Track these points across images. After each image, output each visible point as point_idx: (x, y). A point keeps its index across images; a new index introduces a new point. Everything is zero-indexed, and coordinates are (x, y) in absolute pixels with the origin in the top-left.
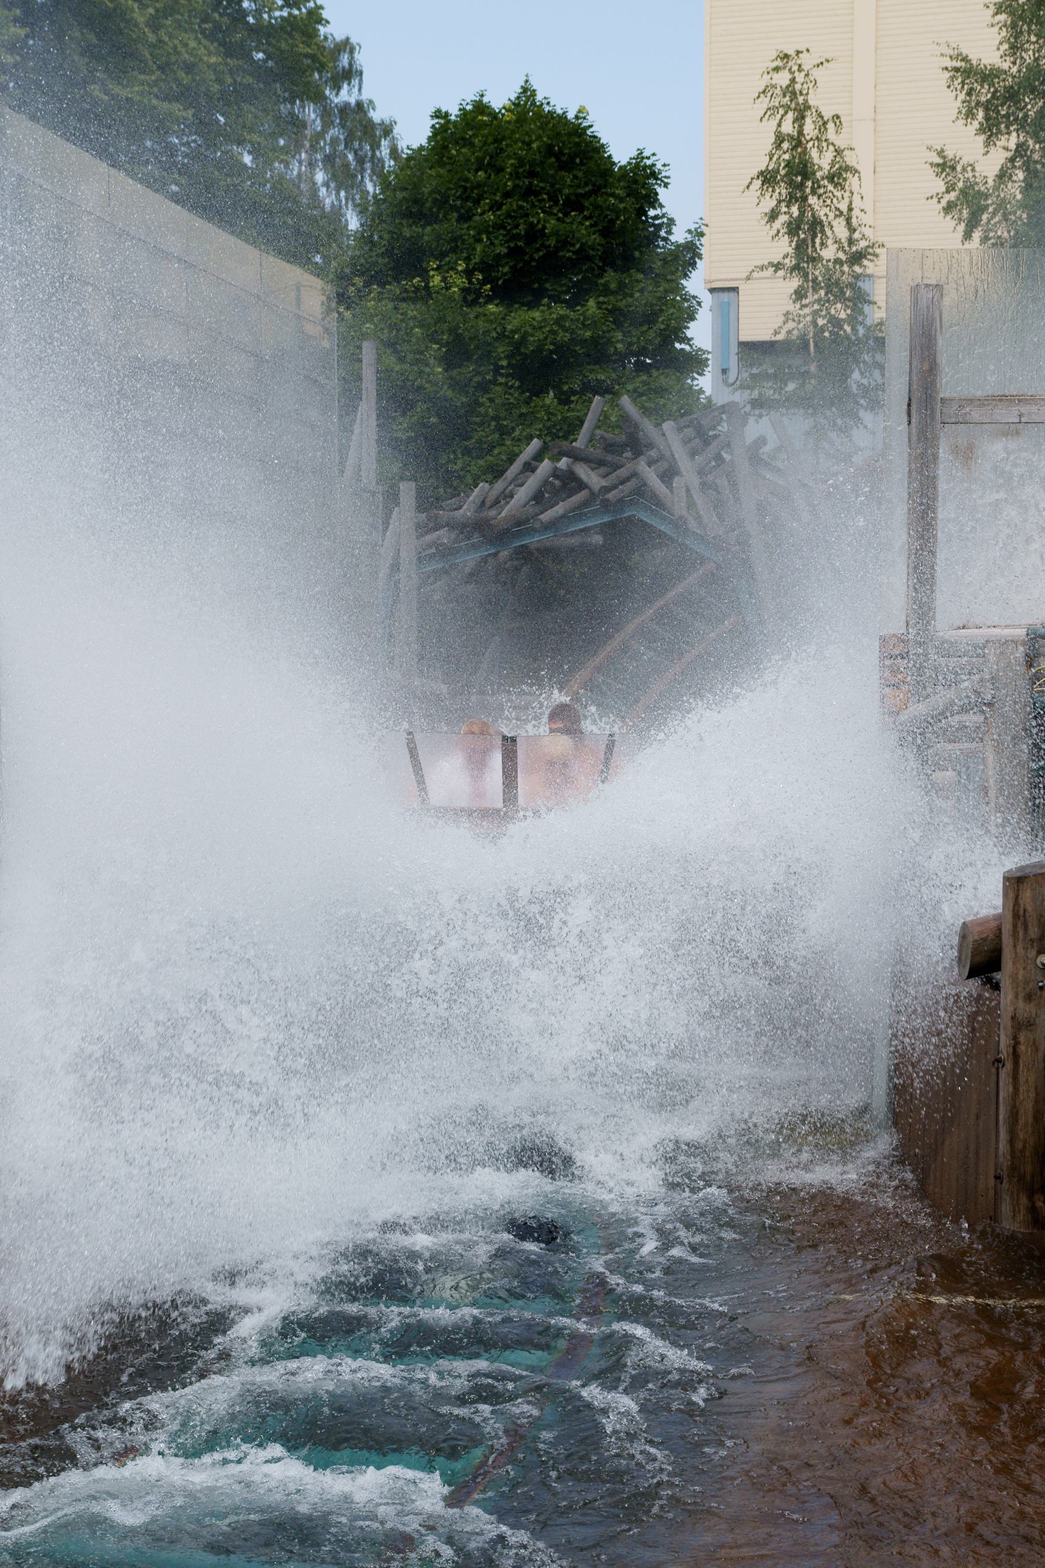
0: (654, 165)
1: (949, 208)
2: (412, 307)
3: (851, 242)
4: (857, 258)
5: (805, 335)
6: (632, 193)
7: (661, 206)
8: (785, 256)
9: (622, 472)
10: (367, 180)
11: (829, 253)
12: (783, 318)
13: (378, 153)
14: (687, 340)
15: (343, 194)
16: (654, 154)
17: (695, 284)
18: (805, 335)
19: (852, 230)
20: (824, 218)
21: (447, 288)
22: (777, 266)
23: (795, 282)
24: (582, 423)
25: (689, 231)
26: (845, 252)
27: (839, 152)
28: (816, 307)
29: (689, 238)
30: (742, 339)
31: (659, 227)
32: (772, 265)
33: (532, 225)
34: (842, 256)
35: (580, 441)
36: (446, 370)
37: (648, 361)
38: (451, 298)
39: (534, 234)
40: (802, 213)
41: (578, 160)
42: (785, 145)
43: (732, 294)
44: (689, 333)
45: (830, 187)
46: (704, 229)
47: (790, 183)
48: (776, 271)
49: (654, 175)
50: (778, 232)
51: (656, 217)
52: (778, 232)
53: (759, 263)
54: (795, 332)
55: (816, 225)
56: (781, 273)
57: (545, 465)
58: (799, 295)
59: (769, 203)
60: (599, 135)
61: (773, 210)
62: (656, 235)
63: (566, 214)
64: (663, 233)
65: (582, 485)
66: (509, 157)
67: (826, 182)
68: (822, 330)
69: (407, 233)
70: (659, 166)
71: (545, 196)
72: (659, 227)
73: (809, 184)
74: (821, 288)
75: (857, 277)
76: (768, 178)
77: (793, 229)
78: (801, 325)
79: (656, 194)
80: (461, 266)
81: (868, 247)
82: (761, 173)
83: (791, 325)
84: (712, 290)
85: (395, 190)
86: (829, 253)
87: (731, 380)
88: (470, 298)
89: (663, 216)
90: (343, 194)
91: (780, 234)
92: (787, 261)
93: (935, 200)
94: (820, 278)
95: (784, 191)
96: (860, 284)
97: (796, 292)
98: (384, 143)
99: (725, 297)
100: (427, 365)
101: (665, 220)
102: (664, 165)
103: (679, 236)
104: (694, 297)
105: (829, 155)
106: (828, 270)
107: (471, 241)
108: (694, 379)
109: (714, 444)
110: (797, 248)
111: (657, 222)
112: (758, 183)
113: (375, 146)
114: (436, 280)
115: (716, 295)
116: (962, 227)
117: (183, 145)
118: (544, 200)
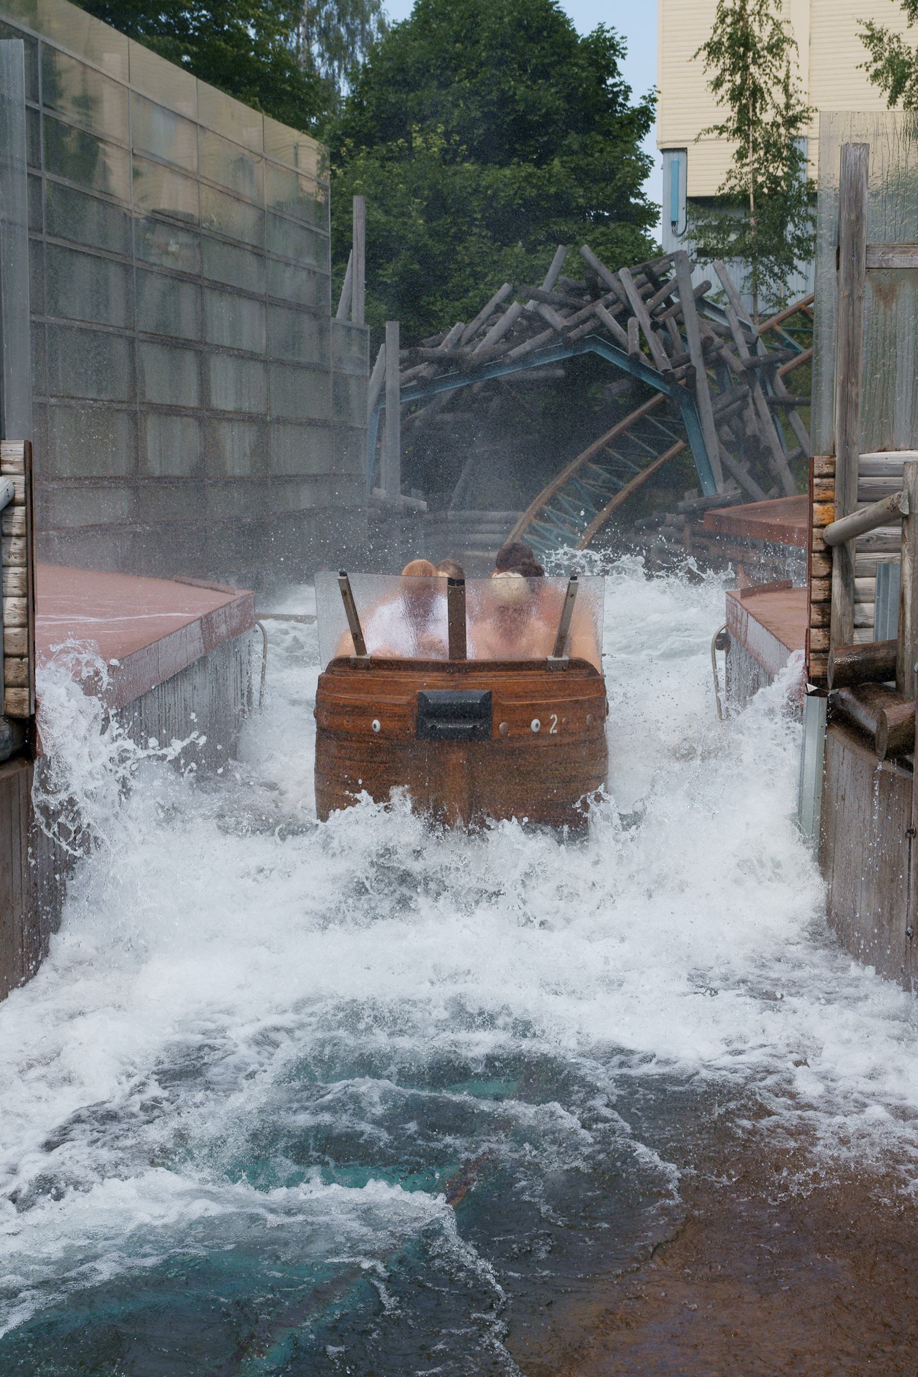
0: (613, 38)
1: (876, 76)
2: (397, 165)
3: (788, 106)
4: (791, 122)
5: (746, 191)
6: (594, 63)
7: (619, 74)
8: (729, 120)
9: (583, 313)
10: (357, 51)
11: (768, 117)
12: (726, 176)
13: (367, 27)
14: (641, 195)
15: (336, 64)
16: (613, 28)
17: (648, 145)
18: (746, 191)
19: (789, 96)
20: (763, 86)
21: (428, 149)
22: (722, 129)
23: (737, 144)
24: (547, 270)
25: (644, 98)
26: (782, 116)
27: (777, 25)
28: (756, 165)
29: (644, 103)
30: (690, 194)
31: (616, 95)
32: (716, 128)
33: (503, 92)
34: (779, 120)
35: (545, 285)
36: (425, 221)
37: (606, 214)
38: (432, 158)
39: (505, 100)
40: (744, 81)
41: (545, 34)
42: (729, 20)
43: (681, 154)
44: (643, 189)
45: (769, 57)
46: (657, 95)
47: (734, 55)
48: (720, 134)
49: (613, 47)
50: (723, 97)
51: (615, 85)
52: (723, 97)
53: (707, 126)
54: (738, 189)
55: (757, 92)
56: (725, 135)
57: (514, 308)
58: (741, 155)
59: (714, 72)
60: (564, 11)
61: (718, 79)
62: (614, 101)
63: (534, 82)
64: (620, 100)
65: (546, 325)
66: (483, 30)
67: (765, 52)
68: (761, 186)
69: (392, 98)
70: (617, 38)
71: (515, 66)
72: (616, 95)
73: (750, 54)
74: (761, 148)
75: (793, 138)
76: (714, 49)
77: (736, 95)
78: (743, 182)
79: (615, 64)
80: (441, 129)
81: (803, 111)
82: (708, 45)
83: (733, 182)
84: (663, 151)
85: (382, 60)
86: (768, 117)
87: (680, 231)
88: (448, 157)
89: (621, 83)
90: (336, 64)
91: (725, 100)
92: (730, 124)
93: (864, 68)
94: (760, 140)
95: (728, 61)
96: (795, 145)
97: (737, 152)
98: (373, 18)
99: (675, 156)
100: (410, 217)
101: (622, 88)
102: (622, 38)
103: (635, 102)
104: (647, 157)
105: (769, 28)
106: (767, 132)
107: (449, 105)
108: (646, 230)
109: (665, 287)
110: (739, 112)
111: (615, 90)
112: (705, 53)
113: (365, 20)
114: (418, 142)
115: (666, 154)
116: (887, 93)
117: (194, 19)
118: (514, 69)
